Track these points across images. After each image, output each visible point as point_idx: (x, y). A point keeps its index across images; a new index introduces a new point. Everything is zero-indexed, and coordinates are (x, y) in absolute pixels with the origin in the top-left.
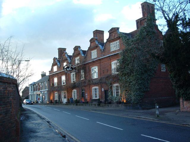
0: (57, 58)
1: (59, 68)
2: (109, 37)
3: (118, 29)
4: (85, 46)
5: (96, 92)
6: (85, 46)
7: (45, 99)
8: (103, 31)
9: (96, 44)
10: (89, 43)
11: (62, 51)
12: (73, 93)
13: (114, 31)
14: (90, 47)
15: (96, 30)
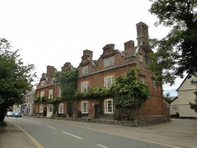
0: (45, 74)
1: (47, 82)
2: (103, 53)
3: (113, 45)
4: (76, 63)
5: (85, 106)
6: (76, 63)
7: (29, 112)
8: (92, 52)
9: (88, 60)
10: (81, 59)
11: (171, 85)
12: (60, 107)
13: (109, 50)
14: (102, 55)
15: (86, 50)
